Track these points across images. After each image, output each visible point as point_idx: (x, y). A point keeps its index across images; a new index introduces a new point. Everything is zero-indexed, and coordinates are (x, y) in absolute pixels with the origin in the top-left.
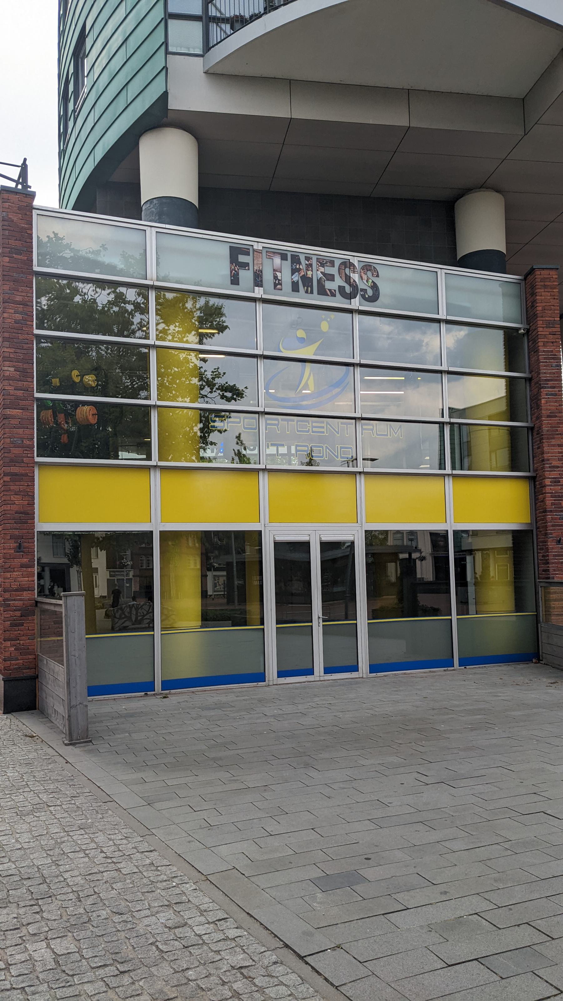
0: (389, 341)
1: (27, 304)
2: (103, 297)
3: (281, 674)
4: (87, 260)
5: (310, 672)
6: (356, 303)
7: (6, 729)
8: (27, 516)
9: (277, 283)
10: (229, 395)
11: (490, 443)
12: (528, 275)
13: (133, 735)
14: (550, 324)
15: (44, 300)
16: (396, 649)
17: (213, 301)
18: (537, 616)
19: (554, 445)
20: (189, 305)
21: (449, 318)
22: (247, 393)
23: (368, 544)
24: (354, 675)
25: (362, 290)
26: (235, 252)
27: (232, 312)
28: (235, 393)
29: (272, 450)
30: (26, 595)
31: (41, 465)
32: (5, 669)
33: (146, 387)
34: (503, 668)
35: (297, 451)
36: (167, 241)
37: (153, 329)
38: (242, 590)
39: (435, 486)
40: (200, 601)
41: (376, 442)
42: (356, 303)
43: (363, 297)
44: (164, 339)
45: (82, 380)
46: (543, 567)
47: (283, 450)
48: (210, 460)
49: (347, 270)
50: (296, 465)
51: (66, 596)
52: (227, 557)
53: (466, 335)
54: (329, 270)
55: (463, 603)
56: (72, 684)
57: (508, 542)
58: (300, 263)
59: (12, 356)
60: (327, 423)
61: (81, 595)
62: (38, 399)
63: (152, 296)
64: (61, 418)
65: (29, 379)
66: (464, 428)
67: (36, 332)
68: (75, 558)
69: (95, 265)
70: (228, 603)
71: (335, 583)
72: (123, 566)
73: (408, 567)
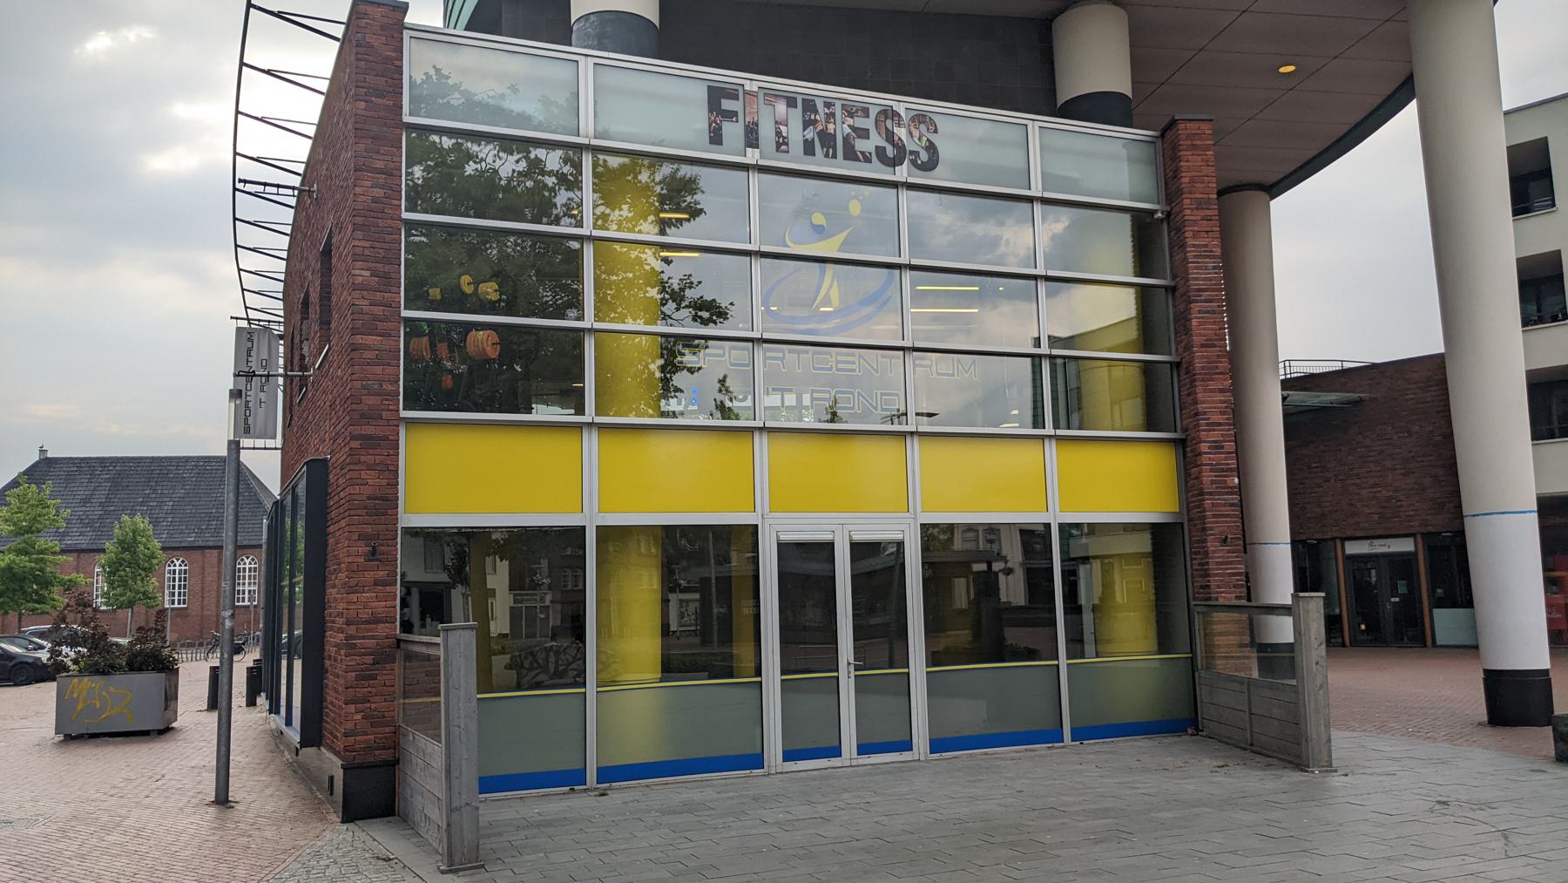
0: (950, 238)
1: (393, 173)
2: (508, 166)
3: (789, 756)
4: (485, 107)
5: (836, 752)
6: (902, 173)
7: (346, 848)
8: (386, 502)
9: (781, 143)
10: (706, 315)
11: (1114, 389)
12: (1167, 130)
13: (551, 856)
14: (1200, 205)
15: (418, 171)
16: (970, 715)
17: (686, 171)
18: (1193, 660)
19: (1212, 391)
20: (644, 177)
21: (1046, 195)
22: (732, 311)
23: (926, 548)
24: (906, 756)
25: (912, 152)
26: (716, 95)
27: (713, 189)
28: (711, 311)
29: (773, 400)
30: (382, 630)
31: (410, 422)
32: (346, 750)
33: (576, 302)
34: (1142, 743)
35: (813, 399)
36: (611, 78)
37: (588, 213)
38: (727, 623)
39: (1027, 455)
40: (659, 640)
41: (934, 387)
42: (902, 173)
43: (914, 163)
44: (602, 228)
45: (476, 289)
46: (1200, 581)
47: (790, 399)
48: (674, 415)
49: (889, 123)
50: (809, 422)
51: (446, 630)
52: (703, 564)
53: (1066, 229)
54: (860, 122)
55: (1076, 643)
56: (455, 774)
57: (1143, 543)
58: (816, 112)
59: (367, 252)
60: (860, 356)
61: (471, 628)
62: (407, 320)
63: (587, 161)
64: (443, 349)
65: (394, 289)
66: (1071, 366)
67: (406, 215)
68: (459, 574)
69: (498, 113)
70: (703, 644)
71: (872, 611)
72: (535, 586)
73: (987, 585)
